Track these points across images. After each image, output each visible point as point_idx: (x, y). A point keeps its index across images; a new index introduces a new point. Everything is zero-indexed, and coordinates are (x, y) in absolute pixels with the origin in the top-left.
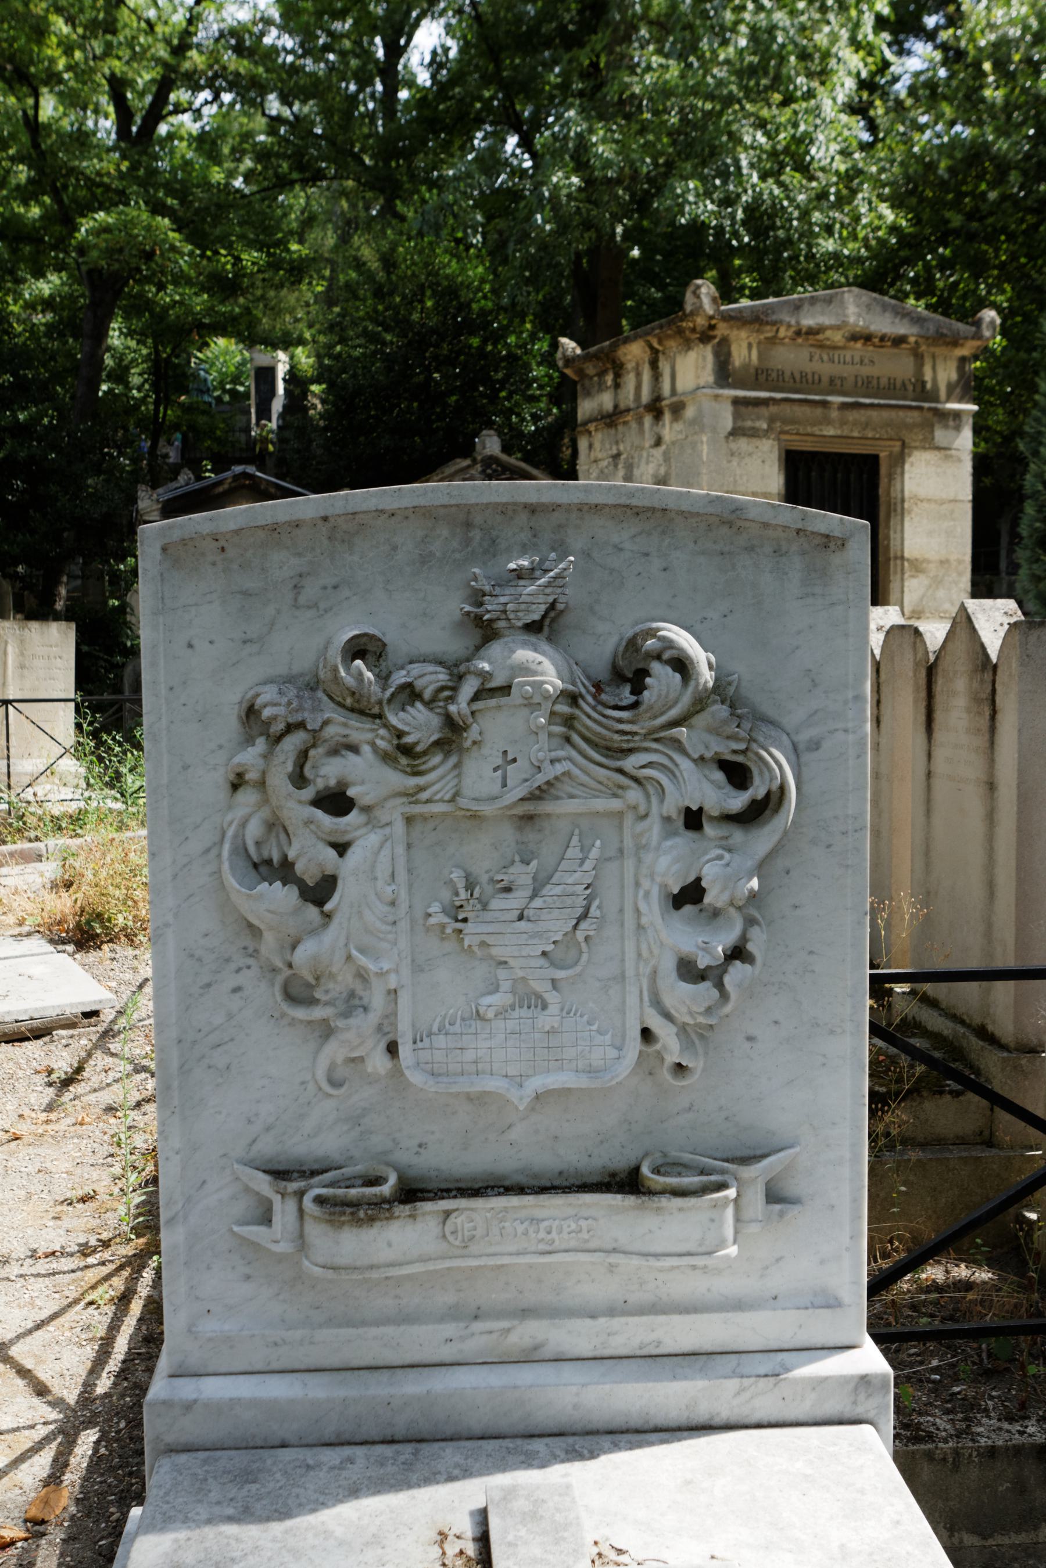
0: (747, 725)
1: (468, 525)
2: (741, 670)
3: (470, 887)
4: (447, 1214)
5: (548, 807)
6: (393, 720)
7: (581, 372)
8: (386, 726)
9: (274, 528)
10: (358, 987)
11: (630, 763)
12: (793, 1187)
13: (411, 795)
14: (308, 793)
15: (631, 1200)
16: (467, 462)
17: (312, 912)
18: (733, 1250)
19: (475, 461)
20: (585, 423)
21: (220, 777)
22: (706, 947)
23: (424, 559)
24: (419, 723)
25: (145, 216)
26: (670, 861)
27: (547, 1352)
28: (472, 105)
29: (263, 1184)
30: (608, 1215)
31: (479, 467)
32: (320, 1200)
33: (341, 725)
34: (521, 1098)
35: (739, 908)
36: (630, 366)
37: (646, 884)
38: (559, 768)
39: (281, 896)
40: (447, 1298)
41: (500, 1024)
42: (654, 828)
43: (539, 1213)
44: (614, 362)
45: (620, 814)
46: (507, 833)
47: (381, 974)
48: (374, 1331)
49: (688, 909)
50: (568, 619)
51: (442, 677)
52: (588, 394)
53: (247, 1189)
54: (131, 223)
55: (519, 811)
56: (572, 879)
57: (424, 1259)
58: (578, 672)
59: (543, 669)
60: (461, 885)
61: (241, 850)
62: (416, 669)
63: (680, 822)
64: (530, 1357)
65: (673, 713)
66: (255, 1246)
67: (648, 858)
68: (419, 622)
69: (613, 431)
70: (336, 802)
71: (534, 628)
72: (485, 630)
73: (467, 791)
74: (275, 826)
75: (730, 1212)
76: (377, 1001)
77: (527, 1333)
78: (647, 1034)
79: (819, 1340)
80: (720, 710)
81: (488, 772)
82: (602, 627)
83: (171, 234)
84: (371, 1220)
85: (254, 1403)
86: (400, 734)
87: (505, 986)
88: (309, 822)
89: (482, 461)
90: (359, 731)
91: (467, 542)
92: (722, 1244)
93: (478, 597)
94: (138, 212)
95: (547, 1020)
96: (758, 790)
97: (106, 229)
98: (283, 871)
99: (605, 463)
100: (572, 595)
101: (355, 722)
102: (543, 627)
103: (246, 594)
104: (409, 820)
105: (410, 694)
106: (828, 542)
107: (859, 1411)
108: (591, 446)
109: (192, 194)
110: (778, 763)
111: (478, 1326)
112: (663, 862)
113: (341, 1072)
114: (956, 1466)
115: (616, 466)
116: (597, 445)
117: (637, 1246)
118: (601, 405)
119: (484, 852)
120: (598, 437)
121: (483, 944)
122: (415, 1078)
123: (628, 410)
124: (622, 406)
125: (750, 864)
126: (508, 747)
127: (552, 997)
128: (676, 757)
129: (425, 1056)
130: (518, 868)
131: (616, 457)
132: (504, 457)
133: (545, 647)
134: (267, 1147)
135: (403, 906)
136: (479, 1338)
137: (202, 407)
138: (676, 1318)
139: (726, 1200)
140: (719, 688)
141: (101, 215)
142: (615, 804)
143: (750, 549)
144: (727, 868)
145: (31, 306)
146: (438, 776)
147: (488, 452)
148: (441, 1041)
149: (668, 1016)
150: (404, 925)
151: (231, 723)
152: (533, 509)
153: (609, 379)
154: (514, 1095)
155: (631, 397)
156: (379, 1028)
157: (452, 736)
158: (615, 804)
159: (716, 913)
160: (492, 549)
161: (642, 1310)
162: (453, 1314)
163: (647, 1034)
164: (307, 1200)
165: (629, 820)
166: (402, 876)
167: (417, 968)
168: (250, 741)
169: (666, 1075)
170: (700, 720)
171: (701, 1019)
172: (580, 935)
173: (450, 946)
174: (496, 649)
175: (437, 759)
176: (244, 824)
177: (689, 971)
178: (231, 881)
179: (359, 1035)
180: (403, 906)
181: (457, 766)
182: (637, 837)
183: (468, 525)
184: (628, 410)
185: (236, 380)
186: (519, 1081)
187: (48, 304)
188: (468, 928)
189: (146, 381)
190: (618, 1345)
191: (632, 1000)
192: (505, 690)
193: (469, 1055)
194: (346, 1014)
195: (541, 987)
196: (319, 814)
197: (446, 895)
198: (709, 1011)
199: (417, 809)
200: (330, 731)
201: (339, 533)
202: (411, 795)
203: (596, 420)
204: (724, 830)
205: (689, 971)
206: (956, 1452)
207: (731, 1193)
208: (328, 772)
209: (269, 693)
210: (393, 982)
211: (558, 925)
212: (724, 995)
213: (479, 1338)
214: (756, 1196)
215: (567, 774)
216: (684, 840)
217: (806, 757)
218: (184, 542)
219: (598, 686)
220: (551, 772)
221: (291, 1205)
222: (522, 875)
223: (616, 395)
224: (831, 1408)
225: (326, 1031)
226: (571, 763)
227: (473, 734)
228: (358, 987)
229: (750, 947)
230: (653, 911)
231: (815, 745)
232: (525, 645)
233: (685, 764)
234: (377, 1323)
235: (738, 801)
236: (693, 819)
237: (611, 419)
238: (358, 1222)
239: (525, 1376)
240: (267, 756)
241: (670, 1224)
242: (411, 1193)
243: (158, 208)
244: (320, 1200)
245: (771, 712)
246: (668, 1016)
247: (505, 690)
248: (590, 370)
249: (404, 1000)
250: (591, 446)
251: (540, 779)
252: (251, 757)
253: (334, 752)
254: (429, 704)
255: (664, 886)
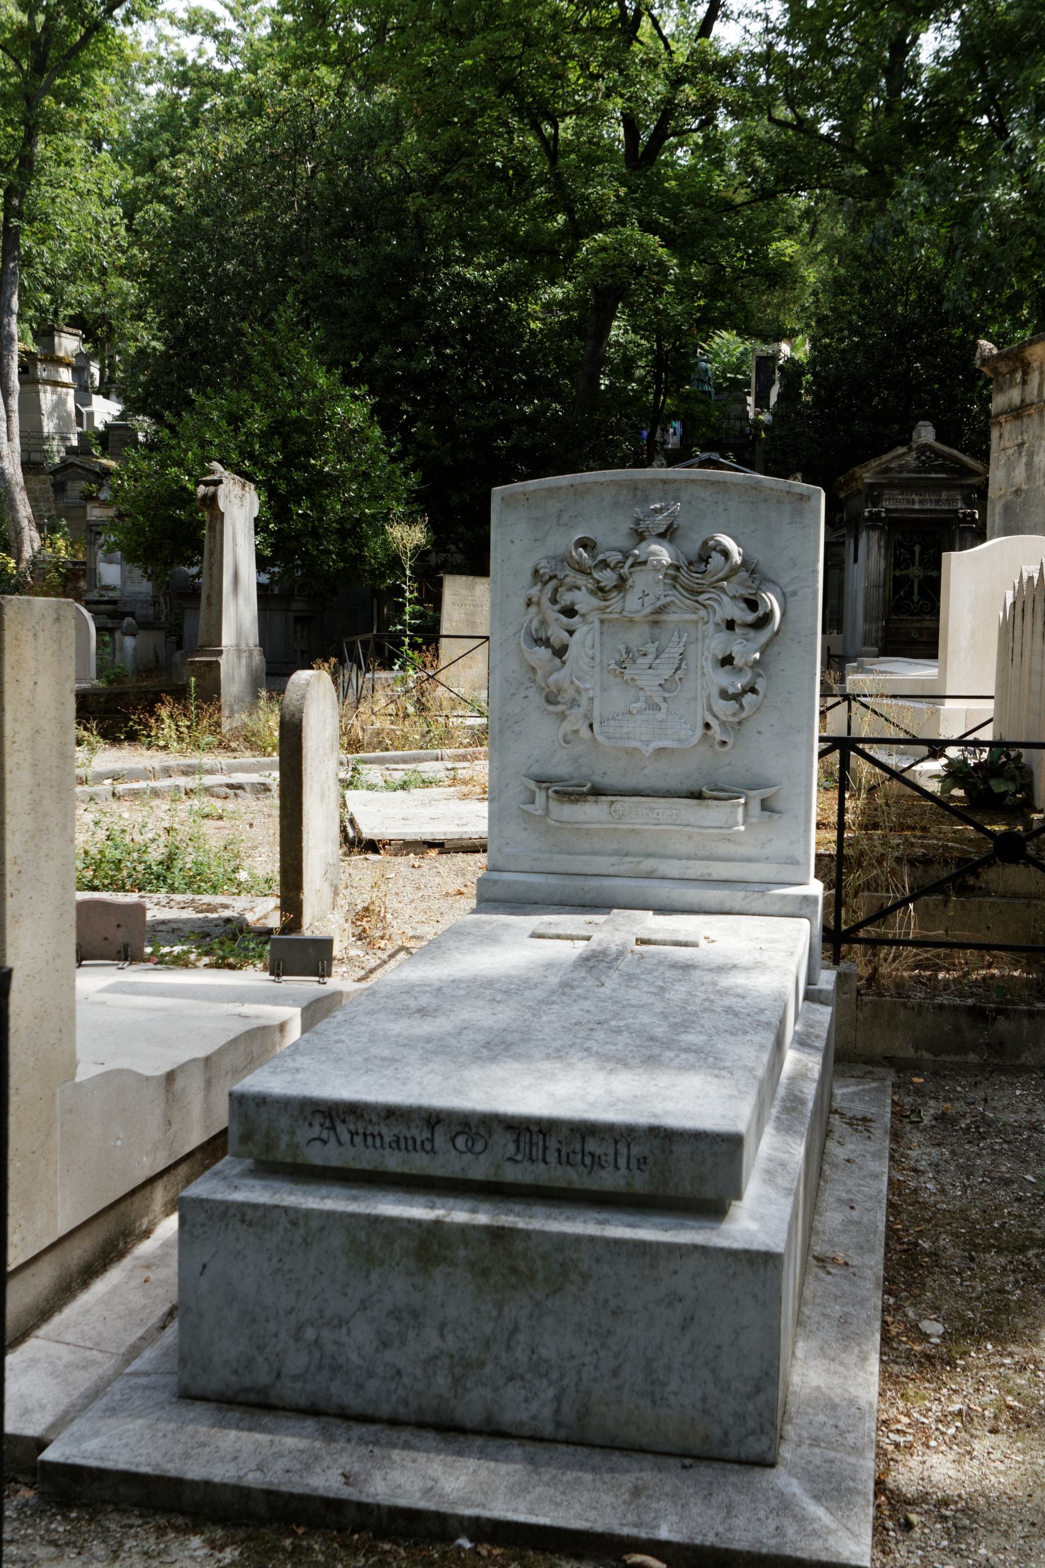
0: (757, 582)
1: (636, 489)
2: (760, 556)
3: (628, 652)
4: (612, 802)
5: (664, 617)
6: (595, 575)
7: (995, 371)
8: (593, 578)
9: (550, 490)
10: (576, 696)
11: (701, 598)
12: (777, 805)
13: (603, 610)
14: (557, 607)
15: (695, 801)
16: (904, 449)
17: (557, 661)
18: (742, 828)
19: (910, 449)
20: (997, 416)
21: (522, 601)
22: (733, 684)
23: (616, 504)
24: (608, 578)
25: (638, 235)
26: (717, 643)
27: (658, 874)
28: (955, 108)
29: (532, 785)
30: (687, 809)
31: (914, 454)
32: (556, 792)
33: (573, 578)
34: (648, 751)
35: (751, 667)
36: (1035, 365)
37: (706, 653)
38: (668, 599)
39: (544, 653)
40: (613, 846)
41: (639, 717)
42: (711, 627)
43: (653, 805)
44: (1022, 361)
45: (696, 622)
46: (646, 629)
47: (586, 690)
48: (579, 857)
49: (727, 667)
50: (679, 532)
51: (619, 557)
52: (1001, 390)
53: (527, 788)
54: (629, 241)
55: (651, 618)
56: (674, 651)
57: (600, 822)
58: (681, 556)
59: (662, 553)
60: (623, 651)
61: (529, 633)
62: (608, 553)
63: (724, 626)
64: (650, 876)
65: (721, 575)
66: (530, 814)
67: (707, 641)
68: (610, 532)
69: (1019, 423)
70: (570, 612)
71: (662, 536)
72: (640, 536)
73: (627, 608)
74: (543, 623)
75: (741, 810)
76: (584, 702)
77: (649, 864)
78: (707, 726)
79: (787, 879)
80: (744, 574)
81: (635, 599)
82: (695, 536)
83: (660, 250)
84: (577, 801)
85: (524, 883)
86: (598, 582)
87: (642, 699)
88: (557, 620)
89: (917, 448)
90: (581, 580)
91: (635, 497)
92: (736, 824)
93: (638, 521)
94: (632, 231)
95: (660, 716)
96: (760, 612)
97: (604, 249)
98: (546, 643)
99: (1011, 451)
100: (681, 521)
101: (579, 576)
102: (667, 535)
103: (537, 519)
104: (602, 621)
105: (604, 564)
106: (802, 498)
107: (803, 912)
108: (1001, 436)
109: (682, 211)
110: (771, 601)
111: (626, 859)
112: (714, 644)
113: (570, 737)
114: (919, 1013)
115: (1020, 454)
116: (1006, 435)
117: (698, 823)
118: (1010, 400)
119: (635, 637)
120: (1007, 428)
121: (633, 679)
122: (600, 739)
123: (1032, 404)
124: (1028, 401)
125: (757, 646)
126: (645, 590)
127: (663, 705)
128: (723, 596)
129: (605, 729)
130: (650, 645)
131: (1021, 445)
132: (938, 445)
133: (666, 544)
134: (536, 770)
135: (598, 660)
136: (626, 865)
137: (702, 397)
138: (718, 863)
139: (739, 804)
140: (744, 563)
141: (599, 236)
142: (694, 617)
143: (766, 500)
144: (747, 650)
145: (548, 307)
146: (615, 601)
147: (923, 440)
148: (612, 723)
149: (716, 716)
150: (597, 668)
151: (528, 575)
152: (665, 482)
153: (1019, 376)
154: (644, 749)
155: (1035, 392)
156: (585, 716)
157: (622, 584)
158: (694, 617)
159: (741, 670)
160: (646, 500)
161: (702, 859)
162: (616, 853)
163: (707, 726)
164: (550, 792)
165: (700, 624)
166: (597, 646)
167: (603, 689)
168: (535, 585)
169: (717, 747)
170: (734, 579)
171: (731, 719)
172: (677, 677)
173: (618, 680)
174: (643, 544)
175: (614, 594)
176: (531, 622)
177: (724, 695)
178: (524, 647)
179: (575, 720)
180: (598, 660)
181: (624, 597)
182: (703, 632)
183: (636, 489)
184: (1032, 404)
185: (737, 369)
186: (647, 743)
187: (564, 305)
188: (626, 671)
189: (648, 372)
190: (691, 873)
191: (699, 708)
192: (645, 563)
193: (625, 730)
194: (570, 708)
195: (658, 700)
196: (562, 616)
197: (617, 656)
198: (734, 714)
199: (605, 616)
200: (568, 580)
201: (579, 492)
202: (603, 610)
203: (1006, 413)
204: (746, 631)
205: (724, 695)
206: (920, 1004)
207: (742, 801)
208: (567, 598)
209: (543, 563)
210: (591, 694)
211: (666, 672)
212: (742, 707)
213: (626, 865)
214: (755, 806)
215: (672, 602)
216: (725, 635)
217: (790, 599)
218: (511, 496)
219: (691, 563)
220: (664, 601)
221: (543, 794)
222: (651, 648)
223: (1023, 390)
224: (789, 909)
225: (563, 716)
226: (676, 597)
227: (630, 582)
228: (576, 696)
229: (757, 687)
230: (709, 666)
231: (794, 594)
232: (656, 543)
233: (725, 599)
234: (581, 854)
235: (751, 617)
236: (730, 625)
237: (1018, 412)
238: (572, 802)
239: (646, 883)
240: (541, 591)
241: (712, 814)
242: (597, 792)
243: (648, 226)
244: (556, 792)
245: (774, 578)
246: (716, 716)
247: (645, 563)
248: (1003, 368)
249: (596, 703)
250: (1001, 436)
251: (659, 603)
252: (534, 591)
253: (570, 589)
254: (613, 569)
255: (714, 656)
